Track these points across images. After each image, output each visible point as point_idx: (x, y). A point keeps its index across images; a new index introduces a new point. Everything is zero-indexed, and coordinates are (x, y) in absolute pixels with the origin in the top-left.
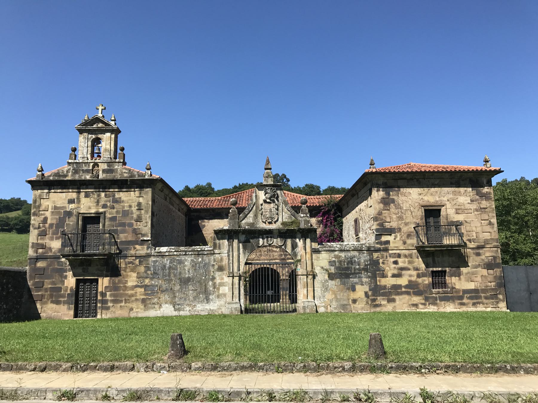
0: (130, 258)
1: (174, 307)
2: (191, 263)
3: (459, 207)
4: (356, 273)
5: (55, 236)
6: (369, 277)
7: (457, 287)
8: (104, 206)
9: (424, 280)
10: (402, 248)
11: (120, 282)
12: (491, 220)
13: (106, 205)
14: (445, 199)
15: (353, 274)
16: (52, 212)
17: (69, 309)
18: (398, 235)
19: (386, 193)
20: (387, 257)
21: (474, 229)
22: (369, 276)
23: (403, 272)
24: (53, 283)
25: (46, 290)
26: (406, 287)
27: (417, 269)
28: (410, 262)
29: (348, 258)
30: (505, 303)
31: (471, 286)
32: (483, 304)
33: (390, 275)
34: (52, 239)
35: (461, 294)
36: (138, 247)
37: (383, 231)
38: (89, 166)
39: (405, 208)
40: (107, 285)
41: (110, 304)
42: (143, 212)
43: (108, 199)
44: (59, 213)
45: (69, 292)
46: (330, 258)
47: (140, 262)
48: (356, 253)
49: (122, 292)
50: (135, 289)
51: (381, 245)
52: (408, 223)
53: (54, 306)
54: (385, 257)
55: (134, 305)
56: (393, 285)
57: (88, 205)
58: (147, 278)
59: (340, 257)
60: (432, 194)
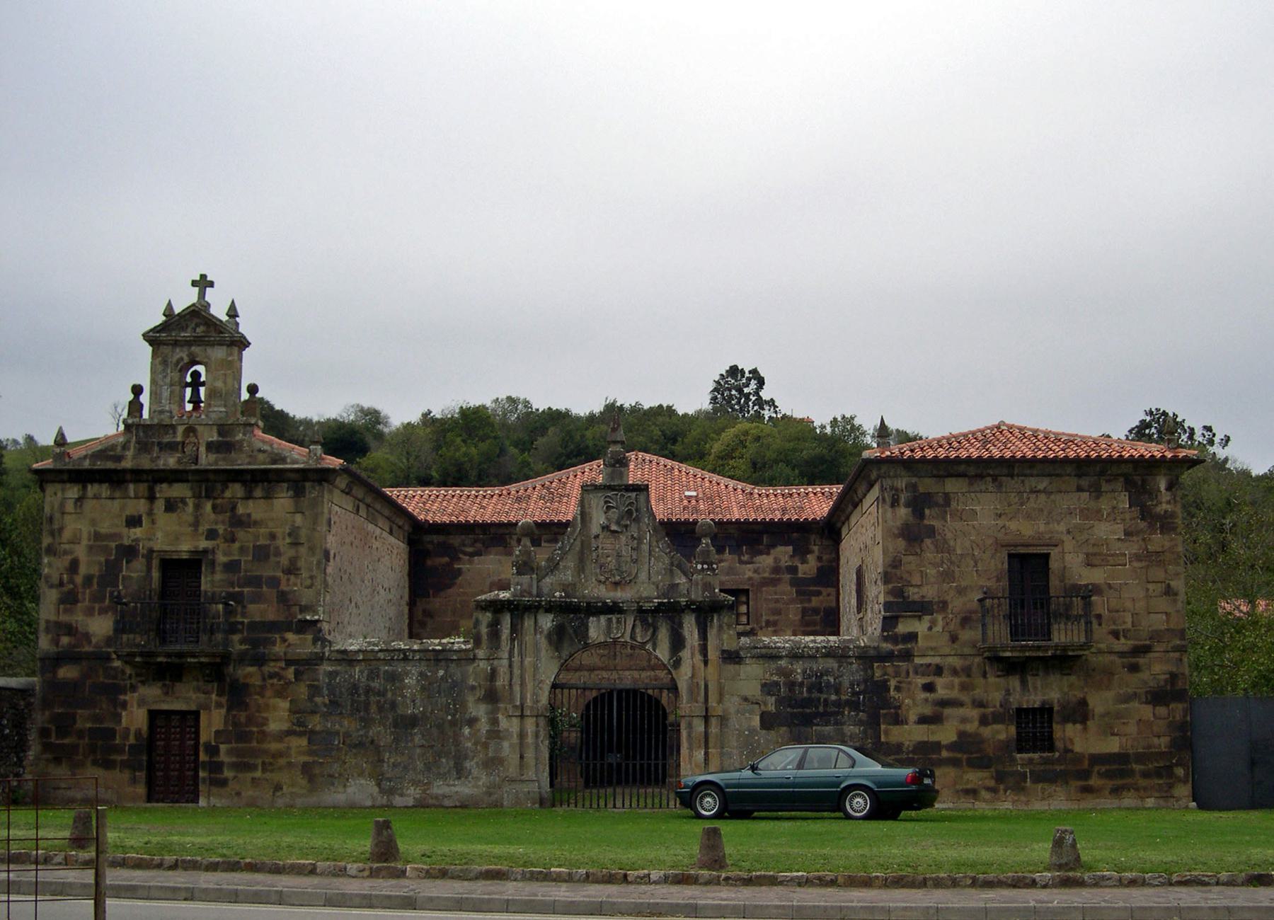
0: (272, 664)
1: (379, 785)
2: (418, 681)
3: (1096, 550)
4: (830, 714)
5: (97, 606)
6: (861, 723)
7: (1078, 748)
8: (212, 534)
9: (998, 732)
10: (947, 651)
11: (250, 720)
12: (1173, 583)
13: (216, 531)
14: (1062, 528)
15: (822, 715)
16: (90, 548)
17: (134, 781)
18: (939, 617)
19: (914, 512)
20: (908, 673)
21: (1129, 604)
22: (860, 721)
23: (947, 711)
24: (97, 718)
25: (80, 735)
26: (952, 747)
27: (980, 704)
28: (964, 687)
29: (810, 677)
30: (1190, 785)
31: (1113, 746)
32: (1137, 790)
33: (913, 717)
34: (90, 612)
35: (1086, 764)
36: (290, 636)
37: (901, 606)
38: (175, 433)
39: (959, 552)
40: (221, 727)
41: (228, 773)
42: (303, 550)
43: (220, 517)
44: (106, 550)
45: (132, 740)
46: (767, 676)
47: (298, 674)
48: (832, 664)
49: (254, 744)
50: (287, 739)
51: (896, 643)
52: (966, 588)
53: (99, 772)
54: (903, 674)
55: (283, 777)
56: (920, 743)
57: (171, 533)
58: (313, 712)
59: (792, 672)
60: (1029, 517)
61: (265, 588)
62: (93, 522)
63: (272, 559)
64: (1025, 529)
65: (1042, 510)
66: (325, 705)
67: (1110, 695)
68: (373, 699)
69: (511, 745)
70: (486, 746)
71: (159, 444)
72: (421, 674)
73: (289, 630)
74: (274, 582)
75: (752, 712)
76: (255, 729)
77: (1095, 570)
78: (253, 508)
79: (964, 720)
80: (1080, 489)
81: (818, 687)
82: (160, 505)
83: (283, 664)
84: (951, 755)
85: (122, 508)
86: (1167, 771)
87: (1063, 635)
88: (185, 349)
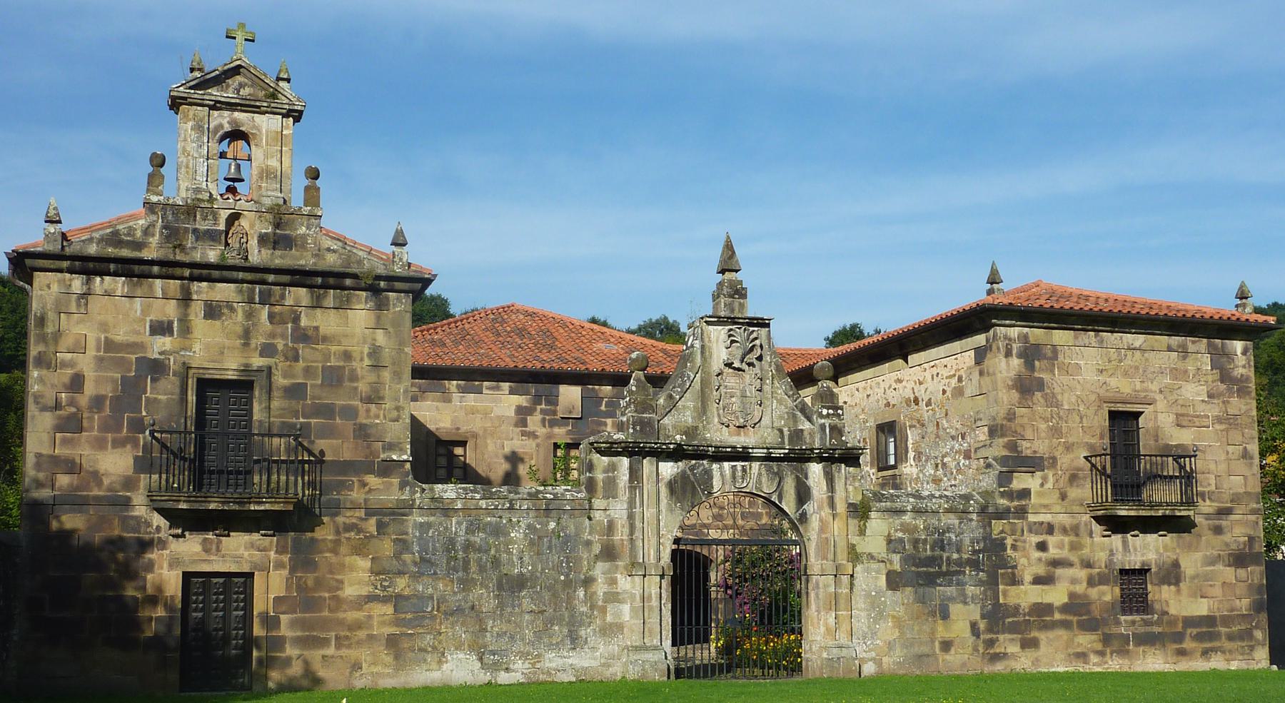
1: (481, 659)
2: (526, 535)
4: (951, 574)
7: (1172, 611)
8: (268, 350)
9: (1104, 594)
11: (319, 583)
14: (1154, 387)
16: (100, 360)
18: (1050, 474)
21: (1212, 466)
22: (980, 580)
23: (1059, 572)
26: (1065, 609)
27: (1088, 564)
28: (1074, 547)
31: (1201, 608)
32: (1224, 652)
33: (1028, 578)
34: (100, 445)
35: (1179, 628)
36: (372, 480)
42: (386, 375)
43: (279, 329)
44: (121, 363)
47: (380, 526)
49: (326, 613)
56: (1035, 604)
58: (400, 573)
60: (1126, 374)
61: (338, 421)
62: (104, 327)
63: (347, 384)
64: (1122, 386)
65: (1137, 368)
66: (415, 563)
67: (1198, 556)
68: (473, 556)
69: (632, 609)
70: (603, 610)
71: (195, 231)
72: (529, 526)
73: (371, 472)
74: (350, 413)
75: (878, 572)
76: (327, 595)
77: (1184, 431)
78: (326, 321)
79: (1074, 581)
80: (1170, 349)
81: (940, 545)
82: (197, 309)
83: (362, 513)
84: (1063, 617)
85: (145, 312)
86: (1246, 635)
87: (1163, 495)
88: (226, 113)
